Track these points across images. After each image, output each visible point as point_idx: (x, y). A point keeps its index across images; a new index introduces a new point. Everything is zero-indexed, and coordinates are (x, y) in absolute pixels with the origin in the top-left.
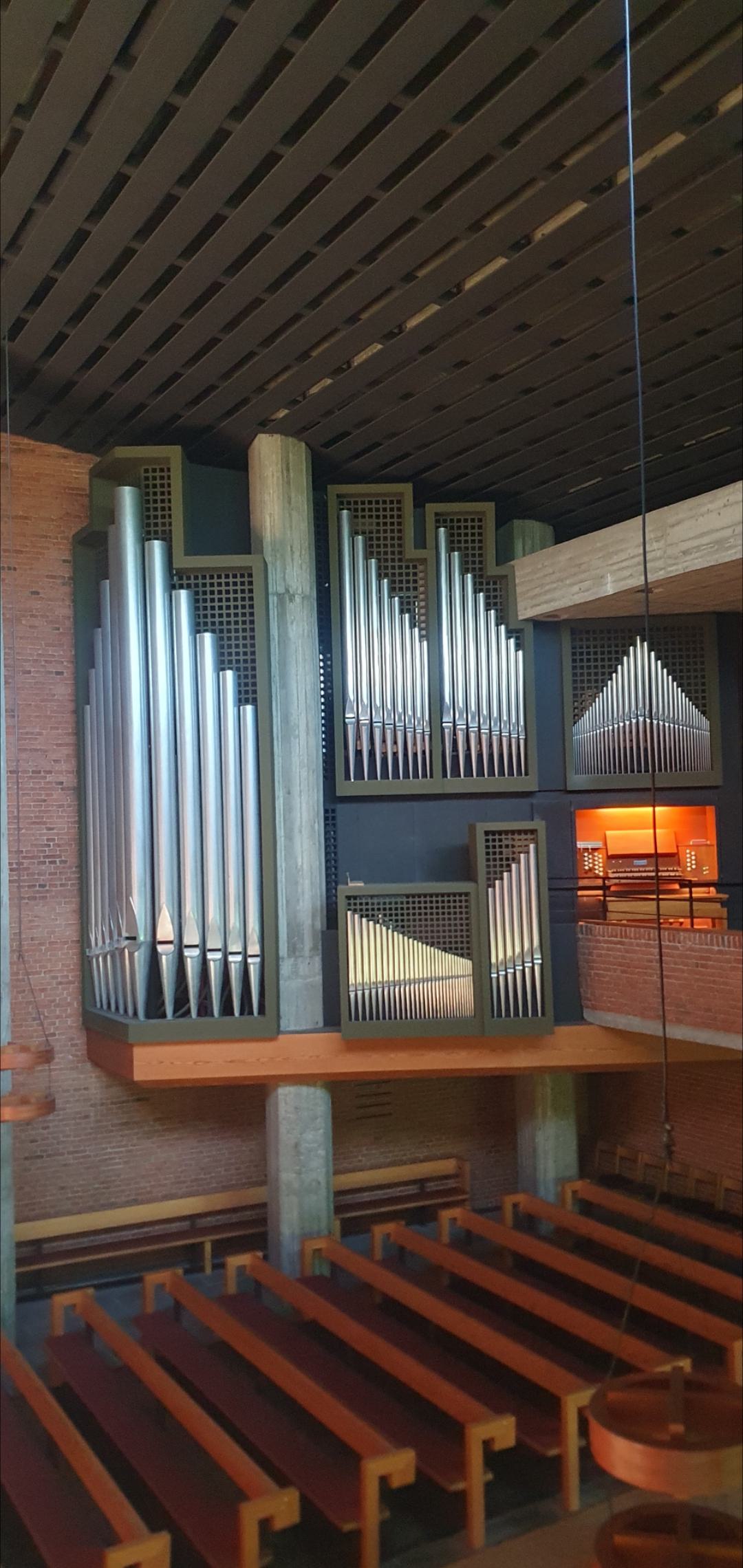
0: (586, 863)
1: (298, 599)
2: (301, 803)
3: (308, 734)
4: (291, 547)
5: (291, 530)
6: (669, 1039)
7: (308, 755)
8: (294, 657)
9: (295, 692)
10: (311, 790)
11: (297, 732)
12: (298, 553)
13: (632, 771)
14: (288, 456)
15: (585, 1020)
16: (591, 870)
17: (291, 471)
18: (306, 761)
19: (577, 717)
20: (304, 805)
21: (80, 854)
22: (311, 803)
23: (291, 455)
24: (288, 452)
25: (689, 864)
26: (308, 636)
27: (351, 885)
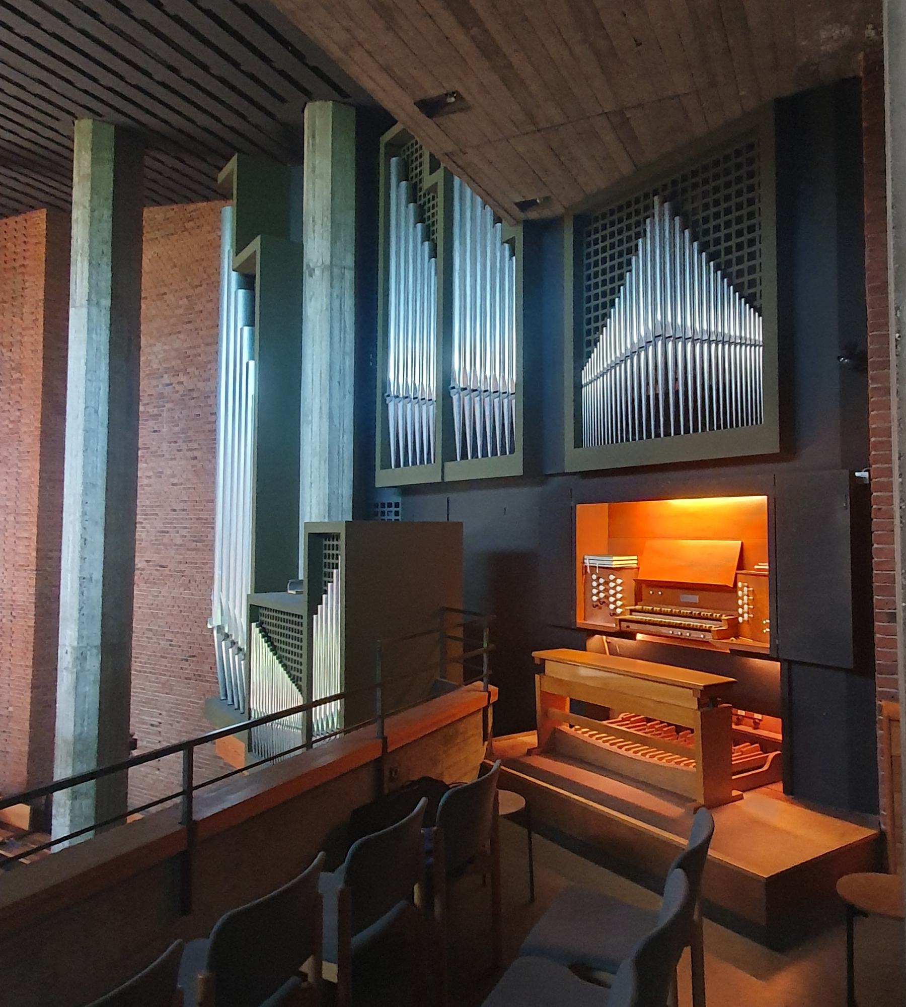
0: (619, 588)
1: (317, 272)
2: (311, 496)
3: (320, 418)
4: (313, 218)
5: (314, 200)
6: (96, 819)
7: (320, 442)
8: (311, 337)
9: (310, 374)
10: (322, 482)
11: (310, 418)
12: (320, 222)
13: (658, 435)
14: (315, 122)
15: (677, 868)
16: (603, 603)
17: (317, 137)
18: (318, 449)
19: (582, 354)
20: (314, 501)
21: (694, 590)
22: (321, 496)
23: (317, 120)
24: (315, 117)
25: (595, 591)
26: (327, 309)
27: (289, 592)
